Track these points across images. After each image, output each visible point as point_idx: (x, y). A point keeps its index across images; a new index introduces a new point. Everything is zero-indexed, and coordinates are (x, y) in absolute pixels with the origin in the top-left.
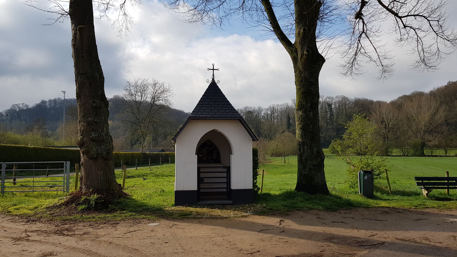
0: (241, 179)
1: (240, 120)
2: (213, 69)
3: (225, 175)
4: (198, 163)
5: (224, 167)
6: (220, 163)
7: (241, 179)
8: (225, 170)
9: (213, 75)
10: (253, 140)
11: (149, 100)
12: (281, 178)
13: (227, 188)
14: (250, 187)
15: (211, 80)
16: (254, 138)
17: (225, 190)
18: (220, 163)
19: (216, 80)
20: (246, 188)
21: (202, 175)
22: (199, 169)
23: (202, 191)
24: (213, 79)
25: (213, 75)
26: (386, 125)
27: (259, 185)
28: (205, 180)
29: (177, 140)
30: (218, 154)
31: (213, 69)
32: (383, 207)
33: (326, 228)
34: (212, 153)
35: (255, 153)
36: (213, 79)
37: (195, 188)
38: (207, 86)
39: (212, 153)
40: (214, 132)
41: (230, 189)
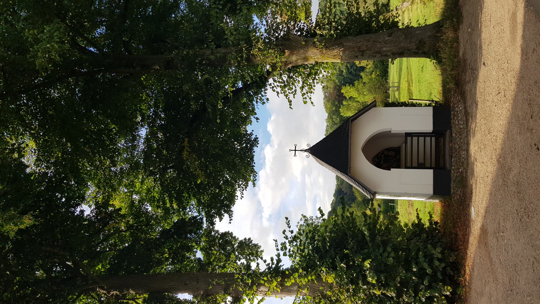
1: (352, 121)
2: (295, 150)
3: (415, 139)
4: (400, 168)
5: (406, 142)
6: (400, 147)
7: (422, 121)
9: (301, 150)
10: (375, 107)
12: (419, 78)
13: (431, 137)
14: (430, 111)
16: (372, 105)
17: (433, 139)
18: (400, 147)
19: (307, 148)
20: (432, 114)
21: (415, 164)
22: (406, 168)
23: (433, 165)
24: (306, 151)
25: (301, 150)
26: (125, 77)
28: (421, 160)
29: (374, 190)
30: (389, 150)
31: (295, 150)
32: (371, 103)
33: (501, 136)
34: (389, 154)
35: (387, 105)
36: (306, 151)
37: (431, 171)
38: (311, 157)
39: (389, 154)
40: (366, 149)
41: (433, 132)
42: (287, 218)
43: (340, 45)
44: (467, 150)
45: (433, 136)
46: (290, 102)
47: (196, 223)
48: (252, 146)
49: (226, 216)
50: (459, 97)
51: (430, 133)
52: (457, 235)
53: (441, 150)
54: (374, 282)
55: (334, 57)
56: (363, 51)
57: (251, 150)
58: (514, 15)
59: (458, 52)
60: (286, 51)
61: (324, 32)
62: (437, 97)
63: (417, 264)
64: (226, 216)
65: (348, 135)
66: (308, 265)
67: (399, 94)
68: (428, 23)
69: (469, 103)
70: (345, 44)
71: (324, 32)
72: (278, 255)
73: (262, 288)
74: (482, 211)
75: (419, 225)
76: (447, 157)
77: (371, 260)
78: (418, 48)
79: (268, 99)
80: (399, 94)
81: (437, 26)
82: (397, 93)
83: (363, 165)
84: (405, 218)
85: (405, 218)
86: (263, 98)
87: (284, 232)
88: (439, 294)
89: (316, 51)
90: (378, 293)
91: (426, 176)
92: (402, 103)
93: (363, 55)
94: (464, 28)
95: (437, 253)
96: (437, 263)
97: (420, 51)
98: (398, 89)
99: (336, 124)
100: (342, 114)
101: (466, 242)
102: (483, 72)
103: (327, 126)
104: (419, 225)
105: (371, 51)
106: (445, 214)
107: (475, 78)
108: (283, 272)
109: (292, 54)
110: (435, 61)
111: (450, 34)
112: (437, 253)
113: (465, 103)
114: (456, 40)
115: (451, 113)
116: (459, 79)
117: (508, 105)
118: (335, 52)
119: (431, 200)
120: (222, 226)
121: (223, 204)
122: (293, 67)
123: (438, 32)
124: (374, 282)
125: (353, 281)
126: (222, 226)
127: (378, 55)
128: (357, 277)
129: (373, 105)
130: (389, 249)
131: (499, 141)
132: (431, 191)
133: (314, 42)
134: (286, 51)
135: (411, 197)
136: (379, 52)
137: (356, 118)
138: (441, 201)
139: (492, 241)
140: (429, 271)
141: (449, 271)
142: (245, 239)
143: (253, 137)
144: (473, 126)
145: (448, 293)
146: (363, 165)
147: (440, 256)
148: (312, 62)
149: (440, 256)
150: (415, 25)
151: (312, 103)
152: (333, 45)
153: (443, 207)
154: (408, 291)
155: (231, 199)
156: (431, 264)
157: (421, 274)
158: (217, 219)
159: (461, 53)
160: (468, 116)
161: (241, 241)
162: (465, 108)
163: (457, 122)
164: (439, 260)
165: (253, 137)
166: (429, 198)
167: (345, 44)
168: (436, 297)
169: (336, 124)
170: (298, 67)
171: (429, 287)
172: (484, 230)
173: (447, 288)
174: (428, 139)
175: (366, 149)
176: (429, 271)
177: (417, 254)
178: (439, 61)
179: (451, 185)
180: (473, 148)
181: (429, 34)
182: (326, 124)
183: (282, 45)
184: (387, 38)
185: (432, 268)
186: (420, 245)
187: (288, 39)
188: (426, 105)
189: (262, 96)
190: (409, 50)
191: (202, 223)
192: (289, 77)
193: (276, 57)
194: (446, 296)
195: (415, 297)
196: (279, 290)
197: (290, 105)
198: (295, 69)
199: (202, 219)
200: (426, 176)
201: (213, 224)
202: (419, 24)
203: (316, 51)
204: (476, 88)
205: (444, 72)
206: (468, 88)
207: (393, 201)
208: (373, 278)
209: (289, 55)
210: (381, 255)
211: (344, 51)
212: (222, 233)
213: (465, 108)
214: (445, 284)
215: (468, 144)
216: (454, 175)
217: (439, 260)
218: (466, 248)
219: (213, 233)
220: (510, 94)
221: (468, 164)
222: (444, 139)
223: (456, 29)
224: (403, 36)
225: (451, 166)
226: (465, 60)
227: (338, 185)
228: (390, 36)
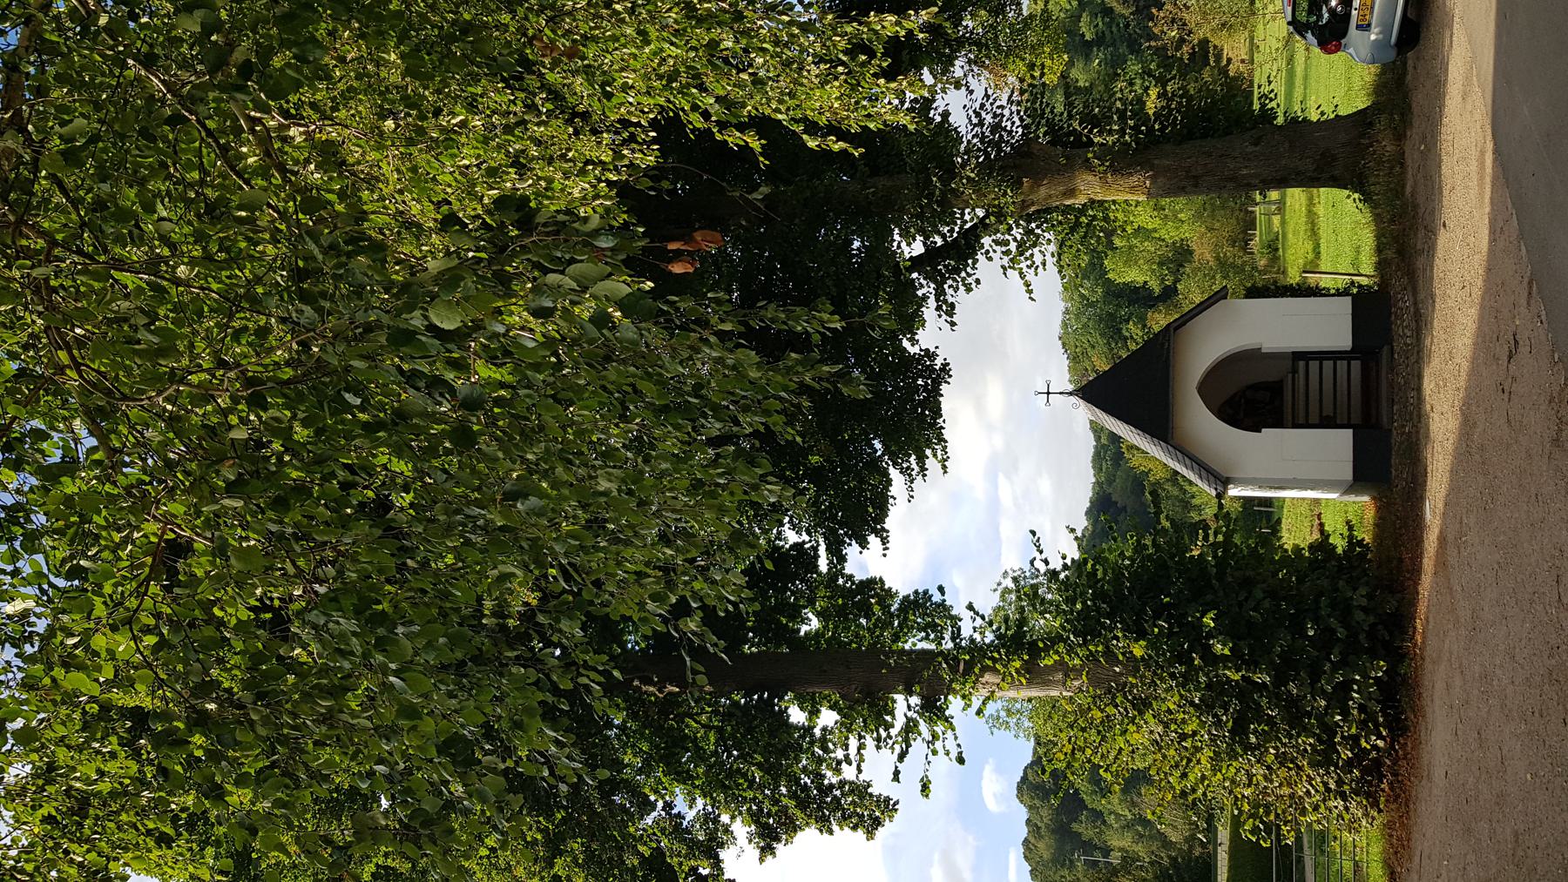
0: (1325, 327)
1: (1176, 329)
3: (1314, 365)
5: (1295, 371)
7: (1325, 327)
8: (1302, 364)
11: (955, 705)
12: (1331, 231)
14: (1347, 302)
15: (1073, 399)
21: (1314, 419)
23: (1356, 418)
24: (1071, 394)
27: (1341, 282)
28: (1328, 411)
30: (1255, 387)
33: (1465, 365)
34: (1260, 394)
35: (1254, 293)
37: (1347, 435)
42: (1033, 533)
44: (1419, 389)
46: (1027, 285)
47: (803, 556)
48: (937, 383)
49: (873, 540)
50: (1405, 280)
52: (1401, 561)
53: (1364, 389)
54: (1227, 652)
55: (1132, 190)
57: (934, 393)
58: (1482, 153)
59: (1404, 186)
61: (1110, 139)
63: (1316, 621)
64: (873, 540)
65: (1168, 358)
66: (1087, 627)
67: (1283, 223)
68: (1343, 112)
69: (1421, 296)
71: (1110, 139)
72: (1021, 610)
73: (988, 677)
74: (1440, 505)
75: (1322, 546)
76: (1384, 403)
79: (978, 282)
80: (1283, 223)
81: (1361, 119)
82: (1276, 220)
83: (1201, 422)
84: (1295, 535)
85: (1295, 535)
86: (970, 280)
87: (1032, 563)
89: (1090, 178)
91: (1337, 445)
92: (1285, 287)
93: (1196, 186)
94: (1414, 134)
95: (1359, 597)
96: (1359, 616)
98: (1279, 209)
99: (1092, 305)
100: (1110, 276)
101: (1417, 571)
102: (1443, 239)
103: (1067, 312)
104: (1322, 546)
106: (1381, 525)
107: (1431, 250)
108: (1033, 644)
109: (1037, 184)
110: (1356, 196)
111: (1388, 146)
112: (1359, 597)
113: (1415, 292)
114: (1400, 160)
115: (1387, 314)
116: (1405, 234)
117: (1474, 311)
118: (1134, 180)
119: (1352, 498)
120: (863, 562)
121: (863, 515)
122: (1038, 211)
123: (1362, 135)
124: (1227, 652)
126: (863, 562)
128: (1191, 650)
129: (1221, 295)
130: (1258, 594)
131: (1464, 374)
132: (1347, 473)
133: (1088, 160)
135: (1307, 490)
136: (1232, 179)
137: (1184, 324)
138: (1374, 498)
139: (1452, 551)
140: (1341, 633)
142: (916, 592)
143: (939, 362)
144: (1428, 342)
147: (1364, 602)
148: (1079, 201)
149: (1364, 602)
150: (1314, 117)
152: (1129, 166)
153: (1378, 509)
155: (881, 504)
156: (1345, 620)
157: (1326, 640)
158: (855, 547)
159: (1408, 189)
160: (1420, 322)
161: (906, 598)
162: (1415, 304)
163: (1402, 330)
164: (1364, 609)
165: (939, 362)
166: (1346, 492)
168: (1356, 682)
169: (1092, 305)
170: (1048, 210)
171: (1343, 663)
172: (1442, 539)
174: (1342, 365)
175: (1207, 388)
176: (1341, 633)
177: (1317, 601)
178: (1367, 198)
179: (1386, 463)
180: (1428, 385)
182: (1061, 306)
183: (1015, 167)
184: (1251, 149)
185: (1347, 626)
186: (1325, 583)
187: (1029, 154)
188: (1339, 293)
189: (969, 275)
191: (817, 557)
192: (1028, 232)
193: (1005, 194)
194: (1376, 678)
195: (1312, 685)
197: (1030, 292)
198: (1042, 215)
199: (815, 549)
200: (1337, 445)
201: (842, 559)
202: (1323, 114)
204: (1432, 267)
205: (1377, 219)
206: (1420, 262)
207: (1267, 502)
208: (1224, 645)
209: (1032, 188)
210: (1240, 605)
211: (1153, 178)
212: (861, 582)
213: (1415, 304)
215: (1420, 377)
216: (1396, 438)
217: (1364, 609)
218: (1416, 583)
219: (841, 581)
220: (1477, 293)
221: (1419, 416)
223: (1400, 137)
224: (1287, 145)
226: (1415, 207)
227: (1098, 483)
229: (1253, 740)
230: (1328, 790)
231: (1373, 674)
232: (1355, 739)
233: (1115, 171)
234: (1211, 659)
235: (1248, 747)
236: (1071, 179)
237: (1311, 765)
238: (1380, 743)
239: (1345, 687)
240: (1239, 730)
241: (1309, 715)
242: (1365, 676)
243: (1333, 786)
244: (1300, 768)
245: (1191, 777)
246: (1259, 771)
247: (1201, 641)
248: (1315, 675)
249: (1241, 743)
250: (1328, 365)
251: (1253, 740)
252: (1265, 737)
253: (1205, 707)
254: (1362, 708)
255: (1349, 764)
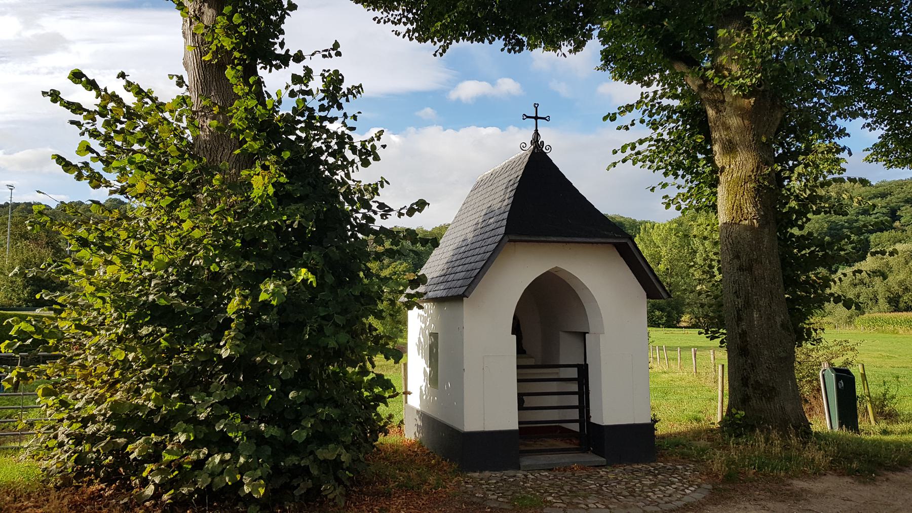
4: (518, 353)
20: (637, 422)
25: (537, 130)
37: (516, 427)
43: (764, 221)
45: (581, 427)
51: (589, 417)
54: (263, 297)
56: (750, 269)
59: (804, 475)
60: (752, 100)
62: (661, 429)
70: (767, 230)
77: (314, 285)
78: (757, 386)
83: (520, 272)
88: (243, 465)
90: (233, 306)
93: (741, 269)
97: (750, 391)
105: (752, 286)
109: (742, 113)
124: (263, 297)
125: (251, 241)
127: (740, 302)
134: (752, 100)
136: (747, 304)
140: (298, 435)
141: (303, 486)
145: (247, 490)
146: (520, 272)
151: (614, 164)
154: (239, 383)
157: (283, 416)
167: (767, 230)
168: (236, 457)
173: (260, 486)
174: (575, 414)
181: (789, 407)
190: (753, 366)
194: (241, 484)
196: (207, 58)
203: (750, 165)
209: (741, 108)
211: (751, 227)
214: (268, 479)
222: (577, 449)
224: (783, 355)
225: (531, 469)
228: (782, 325)
229: (144, 331)
230: (85, 422)
231: (247, 480)
232: (155, 457)
233: (758, 191)
234: (252, 282)
235: (134, 326)
236: (748, 148)
237: (115, 405)
238: (150, 490)
239: (223, 443)
240: (159, 314)
241: (184, 398)
242: (243, 470)
243: (91, 429)
244: (112, 386)
245: (85, 253)
246: (103, 338)
247: (278, 268)
248: (234, 404)
249: (138, 316)
250: (575, 400)
251: (144, 331)
252: (149, 344)
253: (188, 273)
254: (199, 464)
255: (121, 455)
